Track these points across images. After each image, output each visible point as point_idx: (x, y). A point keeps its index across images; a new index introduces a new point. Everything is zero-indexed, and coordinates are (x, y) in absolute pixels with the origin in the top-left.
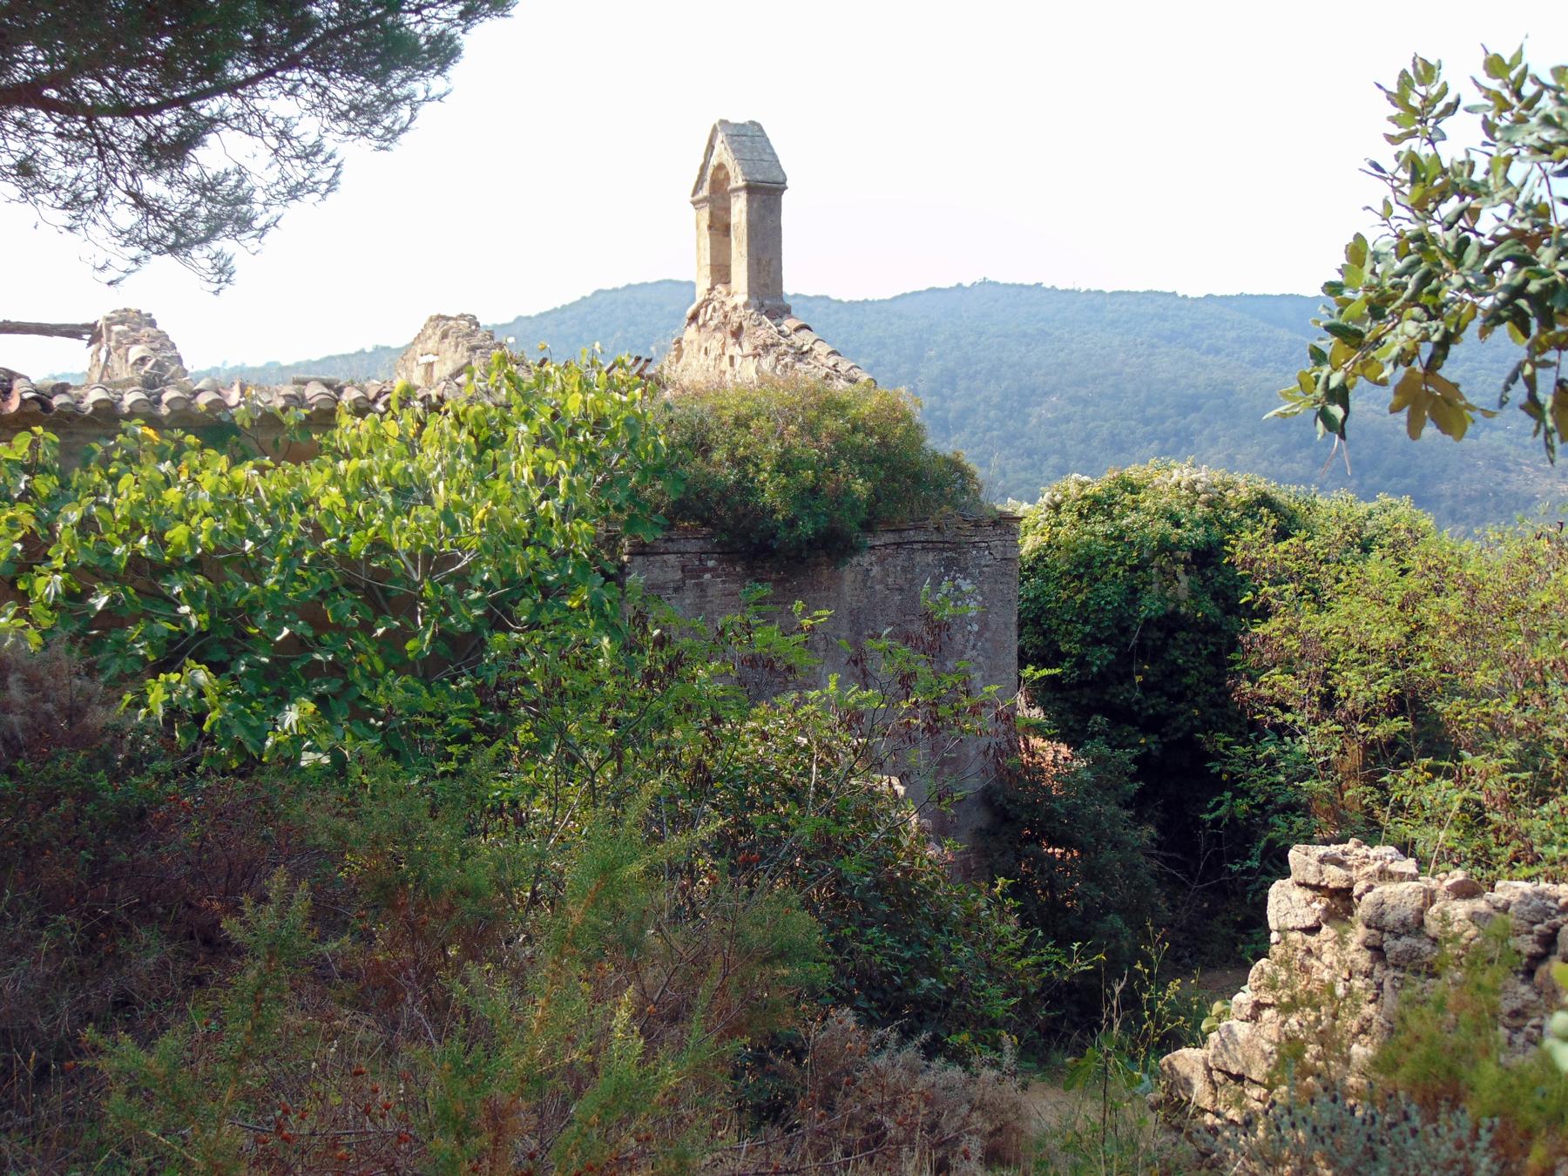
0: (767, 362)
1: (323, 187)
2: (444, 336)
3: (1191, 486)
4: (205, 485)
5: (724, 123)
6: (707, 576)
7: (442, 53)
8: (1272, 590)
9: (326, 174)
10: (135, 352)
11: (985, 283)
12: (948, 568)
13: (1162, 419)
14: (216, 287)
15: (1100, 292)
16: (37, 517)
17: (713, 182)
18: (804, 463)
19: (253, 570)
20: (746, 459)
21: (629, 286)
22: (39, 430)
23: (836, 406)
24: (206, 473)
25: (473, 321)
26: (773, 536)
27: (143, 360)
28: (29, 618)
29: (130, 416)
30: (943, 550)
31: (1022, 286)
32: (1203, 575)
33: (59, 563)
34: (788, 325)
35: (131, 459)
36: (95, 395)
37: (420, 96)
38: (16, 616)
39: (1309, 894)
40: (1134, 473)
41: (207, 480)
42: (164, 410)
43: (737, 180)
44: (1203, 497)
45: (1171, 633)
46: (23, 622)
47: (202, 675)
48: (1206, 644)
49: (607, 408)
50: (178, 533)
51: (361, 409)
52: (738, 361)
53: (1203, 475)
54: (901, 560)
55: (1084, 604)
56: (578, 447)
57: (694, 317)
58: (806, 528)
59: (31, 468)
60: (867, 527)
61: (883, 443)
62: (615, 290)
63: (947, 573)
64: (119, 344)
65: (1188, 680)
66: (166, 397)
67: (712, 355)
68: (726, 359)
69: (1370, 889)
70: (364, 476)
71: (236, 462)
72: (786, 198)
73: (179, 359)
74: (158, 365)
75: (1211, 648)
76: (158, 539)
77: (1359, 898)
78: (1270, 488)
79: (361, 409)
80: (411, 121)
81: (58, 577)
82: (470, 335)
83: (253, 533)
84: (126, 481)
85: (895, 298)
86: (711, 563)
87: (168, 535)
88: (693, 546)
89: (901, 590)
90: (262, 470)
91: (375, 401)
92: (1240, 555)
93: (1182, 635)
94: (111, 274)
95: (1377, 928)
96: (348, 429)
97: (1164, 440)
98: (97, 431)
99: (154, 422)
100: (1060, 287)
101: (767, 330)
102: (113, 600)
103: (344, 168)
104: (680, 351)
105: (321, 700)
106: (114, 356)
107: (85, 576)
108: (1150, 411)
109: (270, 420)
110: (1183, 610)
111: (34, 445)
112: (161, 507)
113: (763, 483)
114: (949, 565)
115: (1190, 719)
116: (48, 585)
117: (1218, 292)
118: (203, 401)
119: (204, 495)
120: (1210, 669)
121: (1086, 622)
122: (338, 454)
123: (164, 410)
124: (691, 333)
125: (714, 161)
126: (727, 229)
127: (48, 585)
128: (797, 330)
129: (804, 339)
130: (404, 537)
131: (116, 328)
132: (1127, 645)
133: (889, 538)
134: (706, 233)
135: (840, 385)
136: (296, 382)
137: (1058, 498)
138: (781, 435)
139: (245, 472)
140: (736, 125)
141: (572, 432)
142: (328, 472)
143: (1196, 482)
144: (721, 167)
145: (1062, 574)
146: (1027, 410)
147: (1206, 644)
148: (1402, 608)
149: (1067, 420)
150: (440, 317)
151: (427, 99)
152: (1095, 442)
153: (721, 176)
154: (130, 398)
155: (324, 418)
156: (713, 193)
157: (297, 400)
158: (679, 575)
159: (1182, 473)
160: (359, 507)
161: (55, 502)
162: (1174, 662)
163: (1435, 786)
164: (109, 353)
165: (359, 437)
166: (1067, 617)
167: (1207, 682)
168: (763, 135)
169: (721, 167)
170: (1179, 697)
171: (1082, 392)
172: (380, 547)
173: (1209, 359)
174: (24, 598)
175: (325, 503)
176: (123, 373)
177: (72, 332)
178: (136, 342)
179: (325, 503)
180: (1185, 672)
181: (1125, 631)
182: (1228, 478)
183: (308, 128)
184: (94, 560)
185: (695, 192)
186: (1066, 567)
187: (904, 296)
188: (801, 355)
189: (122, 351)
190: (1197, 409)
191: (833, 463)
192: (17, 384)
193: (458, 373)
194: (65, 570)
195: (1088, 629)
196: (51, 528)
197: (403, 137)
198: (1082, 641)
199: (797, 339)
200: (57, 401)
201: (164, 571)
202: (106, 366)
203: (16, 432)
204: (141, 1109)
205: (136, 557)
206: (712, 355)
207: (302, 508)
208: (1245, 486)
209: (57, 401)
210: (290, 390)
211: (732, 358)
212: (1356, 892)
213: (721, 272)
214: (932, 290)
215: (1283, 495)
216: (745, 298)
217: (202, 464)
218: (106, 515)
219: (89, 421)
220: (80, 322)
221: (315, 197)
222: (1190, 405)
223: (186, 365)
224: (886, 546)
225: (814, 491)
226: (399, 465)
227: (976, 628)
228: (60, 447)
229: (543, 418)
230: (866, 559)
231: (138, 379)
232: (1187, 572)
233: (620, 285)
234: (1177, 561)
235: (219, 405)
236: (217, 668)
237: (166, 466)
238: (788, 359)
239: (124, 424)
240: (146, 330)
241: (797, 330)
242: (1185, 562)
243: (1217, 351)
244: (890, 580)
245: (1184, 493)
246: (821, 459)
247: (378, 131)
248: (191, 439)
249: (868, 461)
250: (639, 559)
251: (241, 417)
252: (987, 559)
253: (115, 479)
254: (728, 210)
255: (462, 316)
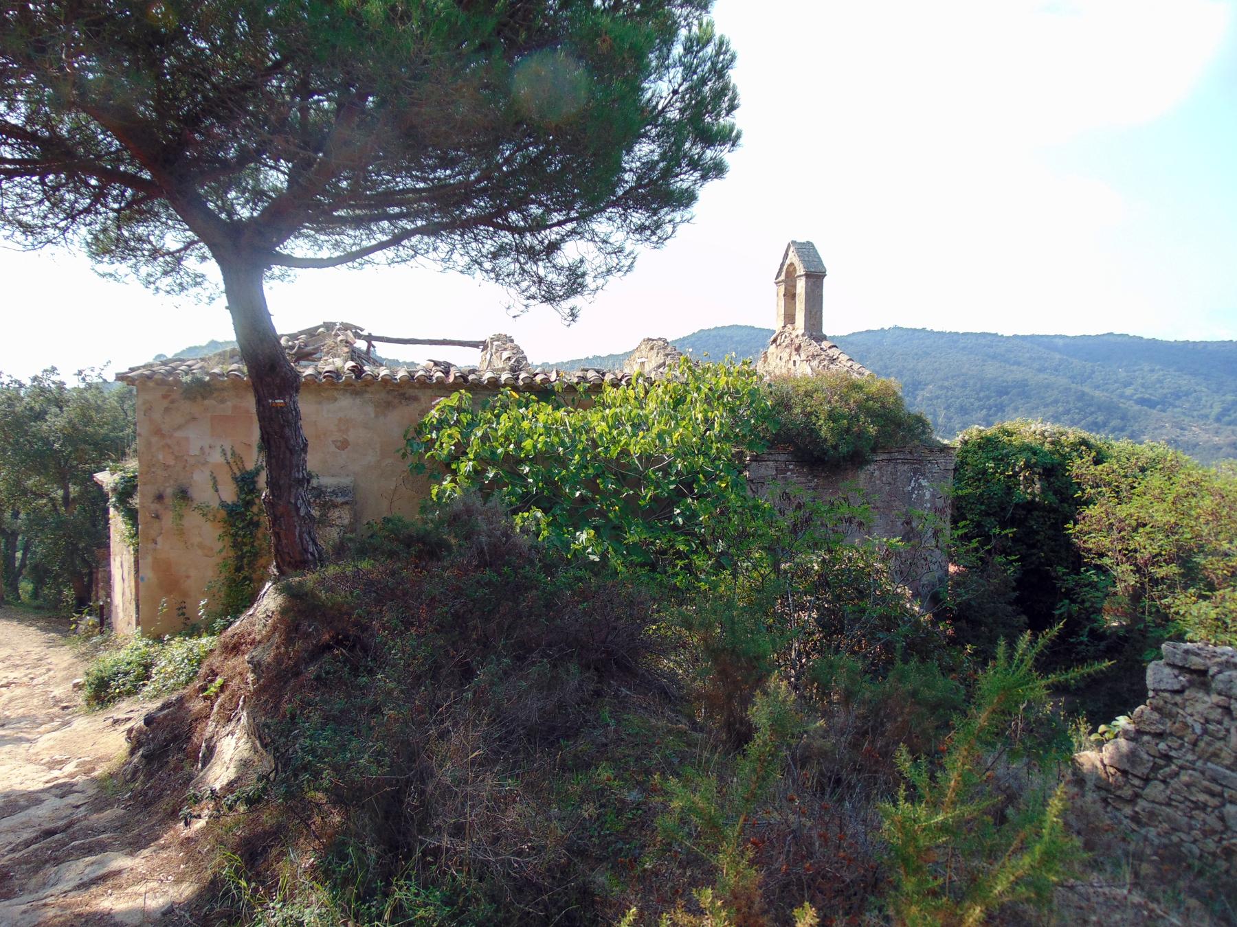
0: (815, 363)
1: (625, 269)
2: (652, 348)
3: (1042, 434)
4: (540, 420)
5: (794, 242)
6: (789, 473)
7: (687, 198)
8: (1093, 491)
9: (627, 262)
10: (506, 355)
11: (896, 328)
12: (915, 473)
13: (988, 398)
14: (567, 323)
15: (957, 333)
16: (461, 433)
17: (787, 272)
18: (843, 417)
19: (563, 462)
20: (811, 413)
21: (716, 328)
22: (463, 391)
23: (856, 387)
24: (542, 414)
25: (665, 341)
26: (825, 454)
27: (509, 359)
28: (456, 483)
29: (505, 385)
30: (913, 463)
31: (915, 330)
32: (1048, 481)
33: (471, 456)
34: (825, 344)
35: (505, 407)
36: (487, 376)
37: (678, 219)
38: (451, 482)
39: (1176, 672)
40: (1008, 425)
41: (542, 417)
42: (521, 383)
43: (800, 271)
44: (1049, 439)
45: (1029, 512)
46: (454, 484)
47: (539, 514)
48: (1049, 518)
49: (739, 385)
50: (528, 444)
51: (615, 384)
52: (797, 364)
53: (1049, 427)
54: (890, 468)
55: (981, 494)
56: (724, 405)
57: (775, 341)
58: (843, 449)
59: (459, 410)
60: (874, 450)
61: (883, 406)
62: (709, 330)
63: (914, 476)
64: (497, 351)
65: (1038, 537)
66: (521, 377)
67: (784, 360)
68: (791, 362)
69: (1220, 672)
70: (617, 417)
71: (556, 408)
72: (825, 280)
73: (525, 358)
74: (517, 361)
75: (1052, 521)
76: (519, 446)
77: (1213, 677)
78: (1085, 434)
79: (615, 384)
80: (673, 232)
81: (471, 463)
82: (665, 348)
83: (562, 443)
84: (504, 417)
85: (849, 335)
86: (791, 467)
87: (523, 444)
88: (782, 457)
89: (890, 484)
90: (568, 413)
91: (621, 380)
92: (1075, 471)
93: (1036, 513)
94: (513, 312)
95: (1226, 696)
96: (610, 394)
97: (990, 409)
98: (488, 393)
99: (515, 388)
100: (935, 330)
101: (814, 347)
102: (496, 475)
103: (638, 260)
104: (766, 357)
105: (596, 528)
106: (494, 356)
107: (485, 460)
108: (982, 395)
109: (571, 388)
110: (1037, 499)
111: (461, 399)
112: (520, 430)
113: (821, 426)
114: (916, 472)
115: (1039, 558)
116: (466, 466)
117: (1020, 333)
118: (538, 379)
119: (540, 425)
120: (1051, 532)
121: (982, 504)
122: (604, 406)
123: (521, 383)
124: (772, 348)
125: (788, 262)
126: (794, 296)
127: (466, 466)
128: (830, 348)
129: (834, 352)
130: (638, 447)
131: (495, 343)
132: (1004, 517)
133: (885, 456)
134: (782, 298)
135: (855, 376)
136: (582, 370)
137: (967, 438)
138: (829, 402)
139: (560, 413)
140: (800, 243)
141: (721, 397)
142: (600, 414)
143: (1046, 431)
144: (792, 264)
145: (969, 478)
146: (917, 392)
147: (1049, 518)
148: (1173, 503)
149: (938, 397)
150: (649, 340)
151: (682, 222)
152: (952, 410)
153: (791, 269)
154: (504, 377)
155: (597, 388)
156: (787, 278)
157: (584, 379)
158: (774, 473)
159: (1036, 426)
160: (615, 432)
161: (472, 425)
162: (1032, 527)
163: (1198, 606)
164: (491, 355)
165: (615, 398)
166: (971, 501)
167: (1049, 538)
168: (814, 248)
169: (792, 264)
170: (1033, 546)
171: (946, 384)
172: (625, 452)
173: (1015, 368)
174: (454, 473)
175: (598, 430)
176: (499, 364)
177: (474, 345)
178: (505, 349)
179: (598, 430)
180: (1037, 533)
181: (1003, 509)
182: (1062, 430)
183: (618, 237)
184: (488, 454)
185: (777, 278)
186: (972, 474)
187: (854, 334)
188: (833, 360)
189: (498, 354)
190: (1007, 393)
191: (857, 417)
192: (452, 369)
193: (659, 367)
194: (474, 460)
195: (983, 507)
196: (468, 441)
197: (668, 241)
198: (980, 514)
199: (831, 352)
200: (471, 377)
201: (521, 462)
202: (490, 361)
203: (452, 392)
204: (563, 760)
205: (507, 453)
206: (784, 360)
207: (587, 432)
208: (1073, 434)
209: (471, 377)
210: (580, 374)
211: (794, 362)
212: (1211, 673)
213: (790, 318)
214: (868, 331)
215: (1095, 438)
216: (803, 331)
217: (539, 409)
218: (494, 434)
219: (485, 387)
220: (478, 340)
221: (621, 274)
222: (1003, 392)
223: (529, 361)
224: (882, 460)
225: (848, 431)
226: (635, 411)
227: (929, 505)
228: (472, 399)
229: (705, 389)
230: (871, 467)
231: (508, 368)
232: (1040, 480)
233: (712, 327)
234: (1034, 473)
235: (546, 380)
236: (545, 511)
237: (523, 410)
238: (826, 363)
239: (502, 390)
240: (509, 344)
241: (830, 348)
242: (1039, 474)
243: (1019, 364)
244: (884, 479)
245: (1038, 437)
246: (850, 414)
247: (654, 238)
248: (533, 397)
249: (874, 415)
250: (754, 463)
251: (557, 386)
252: (936, 469)
253: (498, 416)
254: (795, 287)
255: (660, 339)
